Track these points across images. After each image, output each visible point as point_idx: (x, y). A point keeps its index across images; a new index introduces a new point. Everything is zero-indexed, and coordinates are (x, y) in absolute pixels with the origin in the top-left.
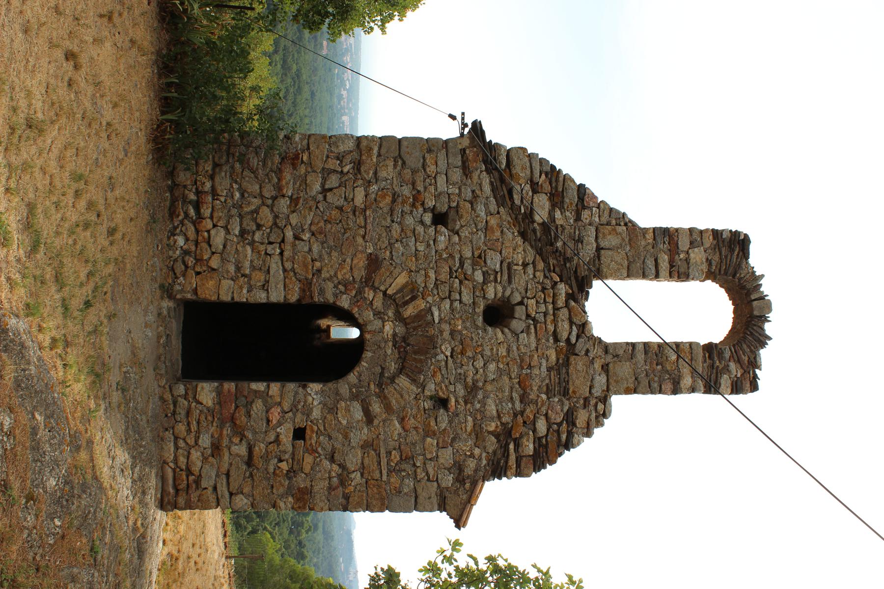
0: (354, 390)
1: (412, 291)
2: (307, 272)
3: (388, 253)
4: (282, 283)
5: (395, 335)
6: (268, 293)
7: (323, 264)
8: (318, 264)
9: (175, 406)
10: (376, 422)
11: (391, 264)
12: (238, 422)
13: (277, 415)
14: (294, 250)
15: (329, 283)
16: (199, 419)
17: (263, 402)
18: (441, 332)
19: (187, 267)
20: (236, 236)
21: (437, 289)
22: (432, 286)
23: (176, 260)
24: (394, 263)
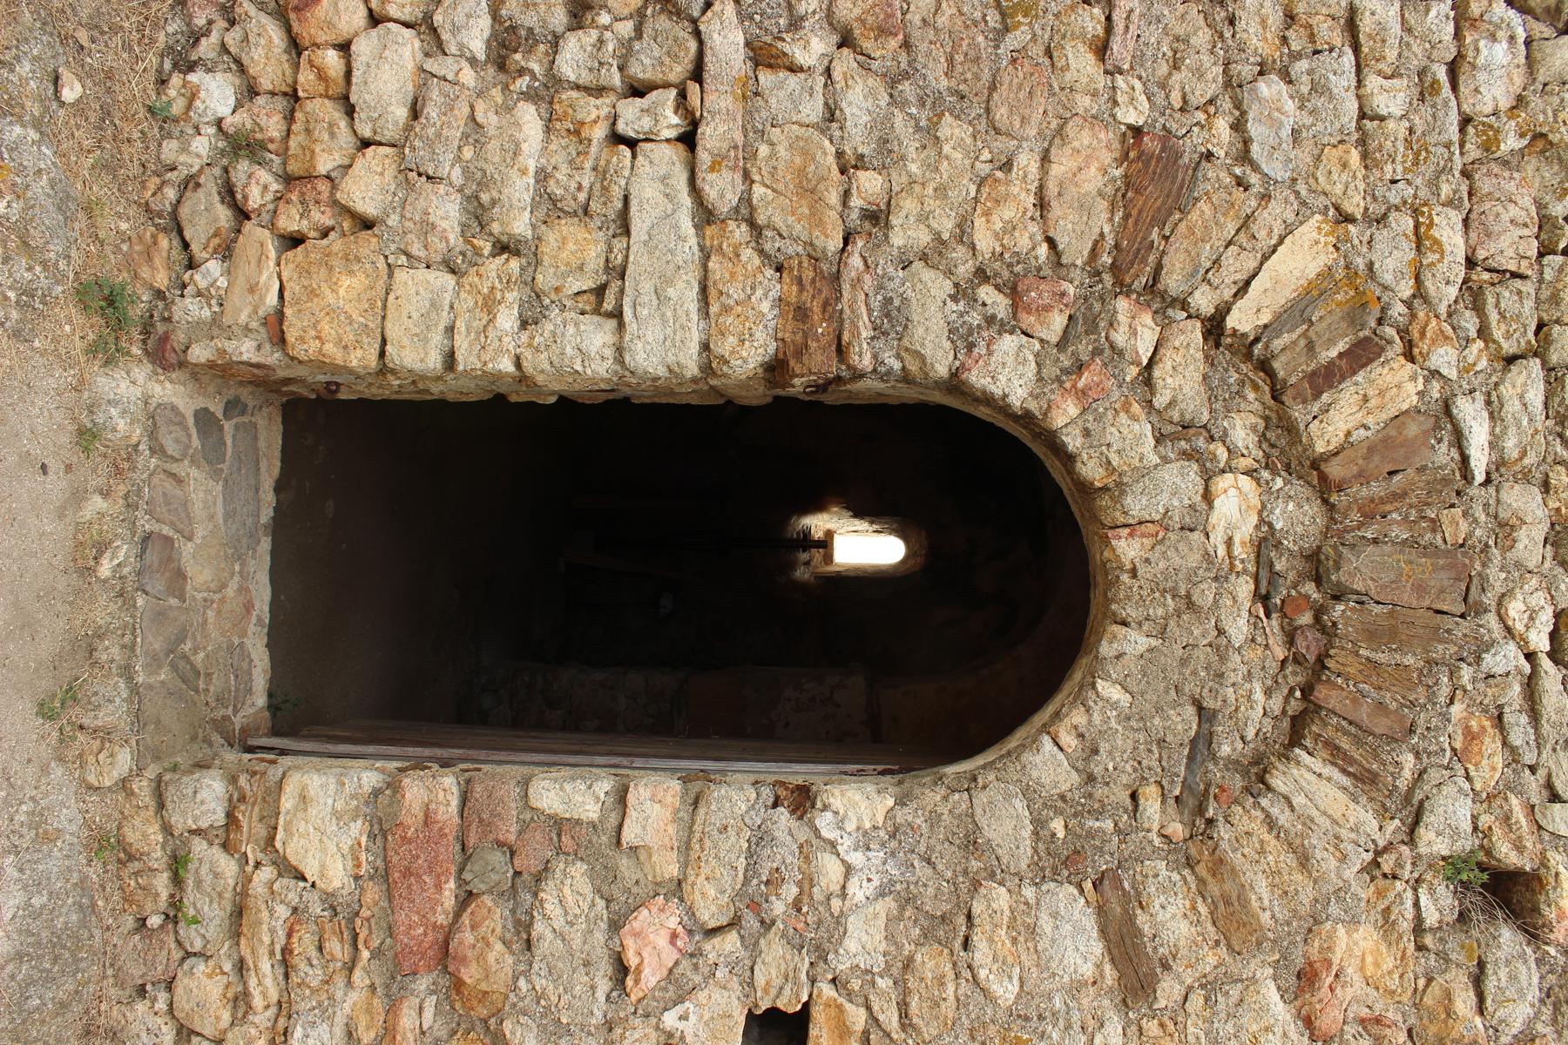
0: (1057, 826)
1: (1356, 312)
2: (816, 220)
3: (1222, 126)
4: (692, 277)
5: (1266, 542)
6: (621, 326)
7: (898, 180)
8: (870, 184)
9: (177, 881)
10: (1168, 991)
11: (1241, 183)
12: (470, 974)
13: (662, 941)
14: (749, 114)
15: (928, 275)
16: (287, 950)
17: (592, 874)
18: (1505, 530)
19: (242, 214)
20: (473, 61)
21: (1478, 308)
22: (1453, 291)
23: (190, 183)
24: (1254, 179)
